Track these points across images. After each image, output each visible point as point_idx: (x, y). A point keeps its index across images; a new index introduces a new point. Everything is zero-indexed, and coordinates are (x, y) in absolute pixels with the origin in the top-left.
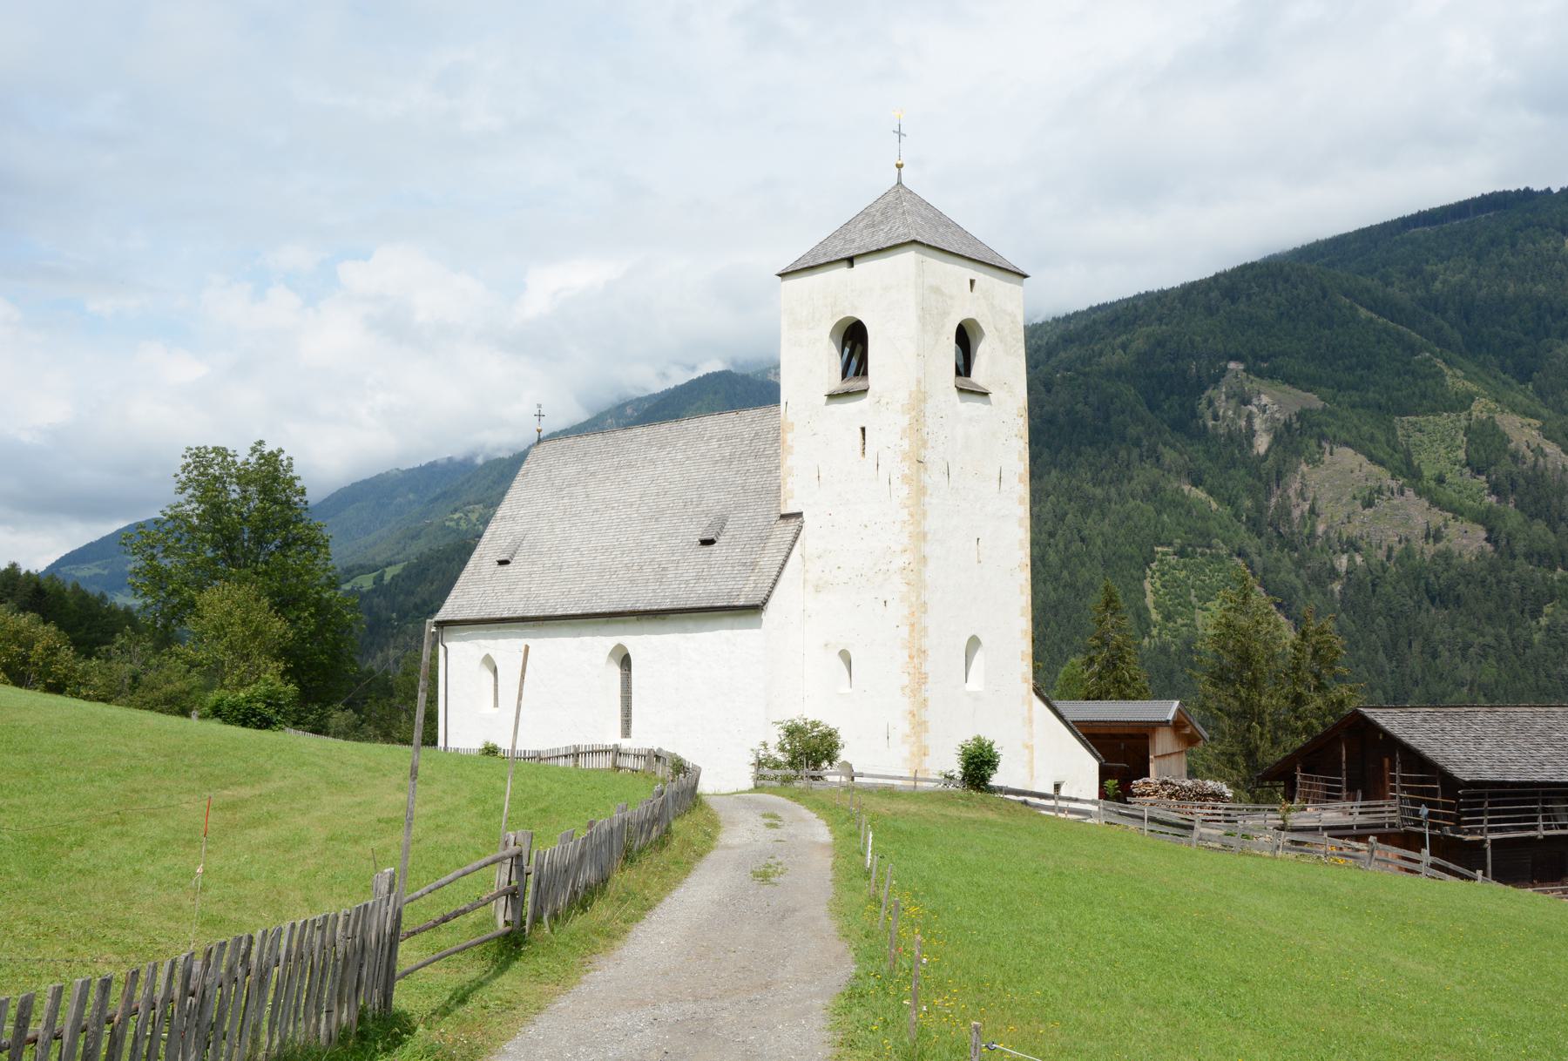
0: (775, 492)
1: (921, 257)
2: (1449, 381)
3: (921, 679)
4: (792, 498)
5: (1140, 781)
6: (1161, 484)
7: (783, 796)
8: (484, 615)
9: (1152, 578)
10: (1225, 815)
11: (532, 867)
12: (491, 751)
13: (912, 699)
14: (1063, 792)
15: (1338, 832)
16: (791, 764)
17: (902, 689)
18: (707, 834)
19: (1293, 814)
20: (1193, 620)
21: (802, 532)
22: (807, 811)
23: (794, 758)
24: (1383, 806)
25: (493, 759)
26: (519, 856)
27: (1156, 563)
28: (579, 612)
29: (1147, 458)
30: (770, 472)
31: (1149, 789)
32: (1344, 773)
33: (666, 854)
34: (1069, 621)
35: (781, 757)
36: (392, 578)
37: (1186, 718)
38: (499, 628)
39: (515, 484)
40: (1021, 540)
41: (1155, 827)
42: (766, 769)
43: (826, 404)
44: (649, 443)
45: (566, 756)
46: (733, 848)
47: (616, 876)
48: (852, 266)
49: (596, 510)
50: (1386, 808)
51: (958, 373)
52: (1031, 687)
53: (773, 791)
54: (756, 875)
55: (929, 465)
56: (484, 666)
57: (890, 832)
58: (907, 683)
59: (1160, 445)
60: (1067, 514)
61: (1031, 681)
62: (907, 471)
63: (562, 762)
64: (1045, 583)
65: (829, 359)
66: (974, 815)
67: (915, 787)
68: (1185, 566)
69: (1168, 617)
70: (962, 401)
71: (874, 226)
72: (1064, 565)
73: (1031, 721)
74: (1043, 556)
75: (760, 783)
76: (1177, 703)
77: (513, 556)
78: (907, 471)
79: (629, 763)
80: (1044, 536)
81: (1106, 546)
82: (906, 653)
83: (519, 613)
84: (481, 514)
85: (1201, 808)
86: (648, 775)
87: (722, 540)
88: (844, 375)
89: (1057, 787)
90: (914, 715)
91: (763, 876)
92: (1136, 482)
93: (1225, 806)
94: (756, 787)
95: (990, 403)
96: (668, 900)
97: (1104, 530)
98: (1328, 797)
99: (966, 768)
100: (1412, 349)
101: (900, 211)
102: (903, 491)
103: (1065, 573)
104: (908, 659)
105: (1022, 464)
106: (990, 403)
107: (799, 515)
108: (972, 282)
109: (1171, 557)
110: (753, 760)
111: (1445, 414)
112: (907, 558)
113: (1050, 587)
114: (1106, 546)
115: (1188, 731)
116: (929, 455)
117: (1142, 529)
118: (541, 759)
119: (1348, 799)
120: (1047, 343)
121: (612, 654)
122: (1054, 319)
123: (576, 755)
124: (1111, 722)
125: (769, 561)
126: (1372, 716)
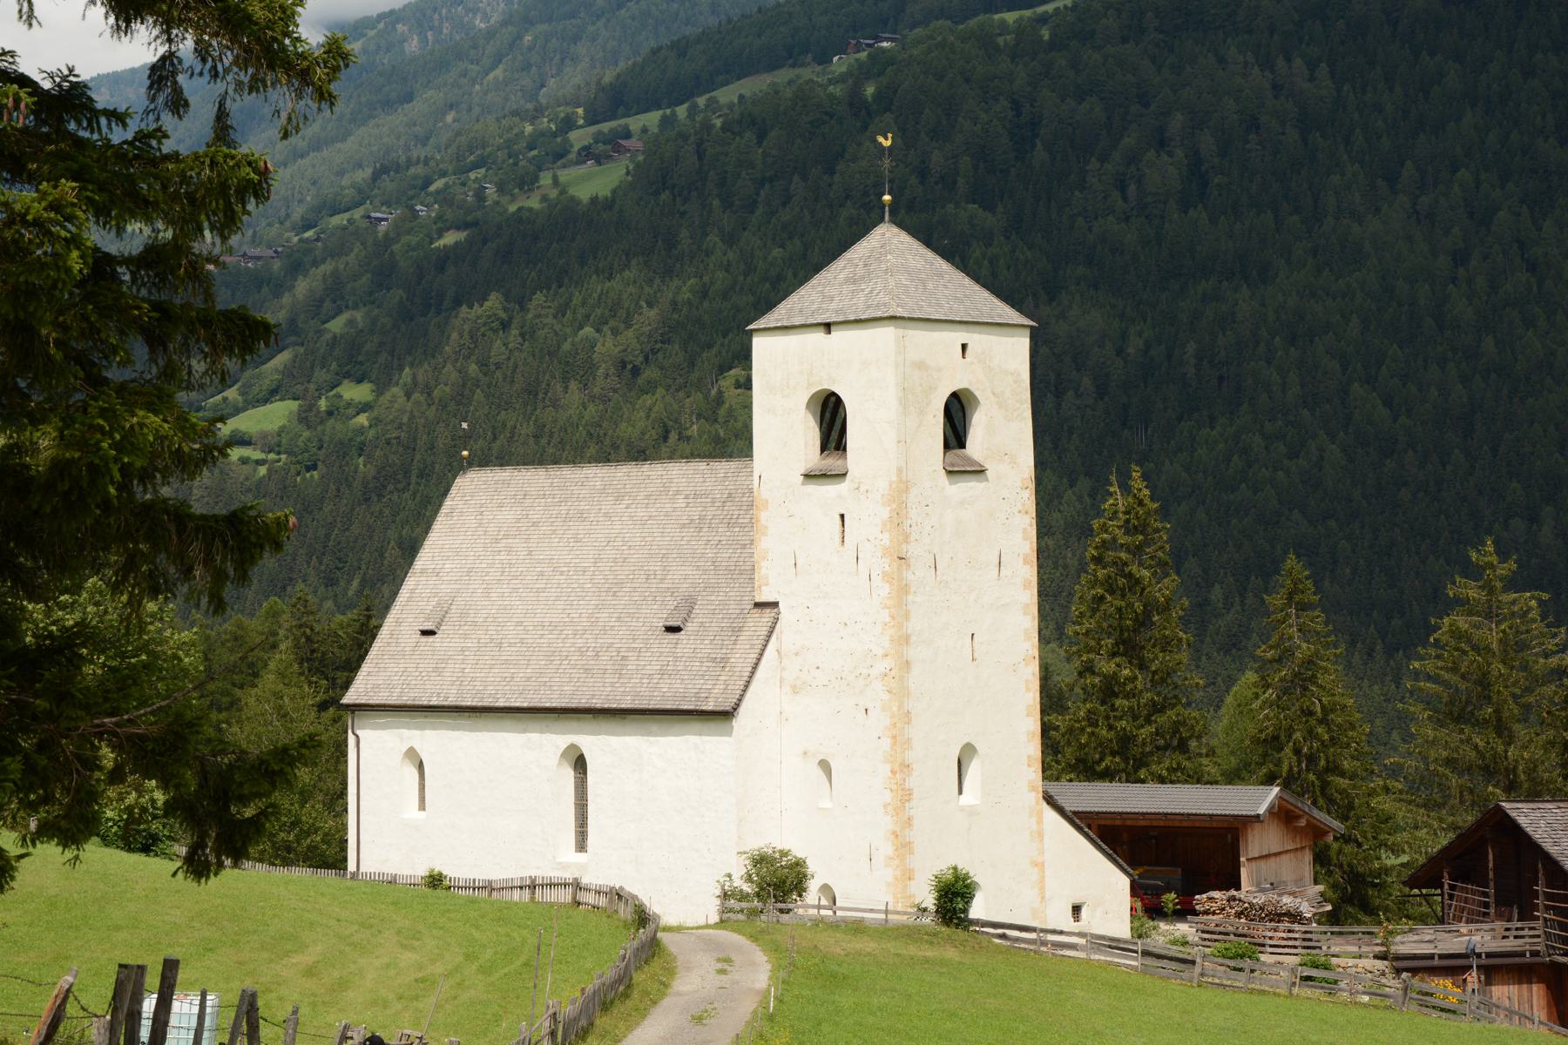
0: (747, 573)
1: (901, 332)
4: (767, 585)
5: (1204, 896)
7: (744, 935)
8: (406, 699)
10: (1304, 940)
12: (435, 881)
15: (1453, 967)
16: (758, 895)
17: (885, 806)
19: (1398, 938)
21: (778, 626)
22: (761, 953)
23: (762, 889)
24: (1522, 929)
25: (439, 892)
26: (555, 1014)
28: (525, 705)
32: (1492, 884)
33: (629, 1003)
35: (747, 888)
42: (732, 901)
43: (803, 484)
45: (521, 888)
47: (597, 1022)
48: (830, 333)
49: (541, 574)
50: (1526, 932)
54: (693, 1017)
57: (830, 977)
62: (887, 568)
63: (516, 895)
65: (809, 431)
66: (930, 953)
67: (886, 920)
71: (854, 282)
73: (1040, 835)
75: (725, 916)
76: (1276, 790)
79: (590, 898)
82: (888, 767)
83: (451, 701)
85: (1275, 931)
86: (611, 914)
87: (690, 627)
88: (823, 448)
89: (1076, 910)
90: (897, 836)
91: (698, 1020)
94: (722, 921)
95: (987, 480)
96: (630, 1036)
99: (939, 899)
102: (884, 590)
103: (1489, 343)
104: (890, 774)
105: (1028, 543)
106: (987, 480)
107: (775, 605)
108: (964, 347)
110: (718, 892)
115: (1303, 823)
116: (912, 550)
119: (1499, 916)
124: (1189, 815)
125: (741, 659)
126: (1513, 814)
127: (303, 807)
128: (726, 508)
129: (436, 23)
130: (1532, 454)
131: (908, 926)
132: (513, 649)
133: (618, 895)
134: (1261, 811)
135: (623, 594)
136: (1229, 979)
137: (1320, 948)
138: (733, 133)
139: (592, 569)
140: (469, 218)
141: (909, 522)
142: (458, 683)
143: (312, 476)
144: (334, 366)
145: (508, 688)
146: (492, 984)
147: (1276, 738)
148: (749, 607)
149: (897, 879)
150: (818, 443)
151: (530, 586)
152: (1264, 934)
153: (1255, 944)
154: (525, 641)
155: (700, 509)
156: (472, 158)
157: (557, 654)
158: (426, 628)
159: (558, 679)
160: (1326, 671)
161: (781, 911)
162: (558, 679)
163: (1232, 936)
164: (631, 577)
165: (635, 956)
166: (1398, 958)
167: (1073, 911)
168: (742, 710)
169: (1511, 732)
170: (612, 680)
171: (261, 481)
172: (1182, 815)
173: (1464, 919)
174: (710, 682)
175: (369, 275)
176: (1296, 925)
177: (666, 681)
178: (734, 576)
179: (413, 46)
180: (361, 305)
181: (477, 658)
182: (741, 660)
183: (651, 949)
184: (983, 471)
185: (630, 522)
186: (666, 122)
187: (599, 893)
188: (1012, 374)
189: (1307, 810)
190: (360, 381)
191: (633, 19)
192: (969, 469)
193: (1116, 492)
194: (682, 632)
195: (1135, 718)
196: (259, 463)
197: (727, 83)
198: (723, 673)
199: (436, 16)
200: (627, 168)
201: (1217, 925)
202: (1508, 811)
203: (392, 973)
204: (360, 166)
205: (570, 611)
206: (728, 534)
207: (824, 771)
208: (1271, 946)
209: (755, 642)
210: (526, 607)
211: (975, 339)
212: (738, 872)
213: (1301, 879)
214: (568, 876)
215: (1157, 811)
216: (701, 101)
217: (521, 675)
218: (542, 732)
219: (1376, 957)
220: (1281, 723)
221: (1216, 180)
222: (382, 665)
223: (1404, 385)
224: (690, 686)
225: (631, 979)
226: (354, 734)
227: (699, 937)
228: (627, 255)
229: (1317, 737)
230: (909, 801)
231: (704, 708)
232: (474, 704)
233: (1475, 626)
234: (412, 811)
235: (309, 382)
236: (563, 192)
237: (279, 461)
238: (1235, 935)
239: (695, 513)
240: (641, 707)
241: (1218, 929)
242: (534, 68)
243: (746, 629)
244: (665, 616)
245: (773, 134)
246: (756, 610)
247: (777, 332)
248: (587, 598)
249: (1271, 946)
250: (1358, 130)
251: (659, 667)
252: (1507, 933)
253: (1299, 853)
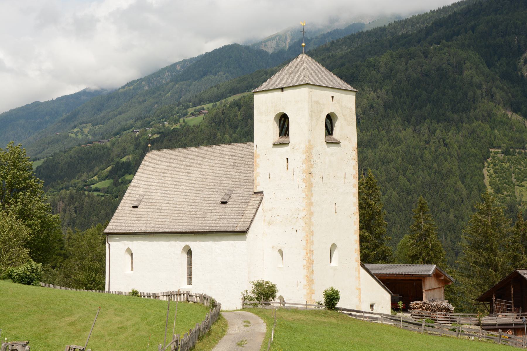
0: (252, 182)
1: (310, 90)
3: (311, 263)
4: (259, 185)
5: (414, 302)
6: (494, 111)
9: (488, 167)
10: (451, 318)
11: (180, 343)
12: (135, 293)
13: (307, 271)
15: (505, 327)
16: (257, 298)
17: (304, 266)
18: (223, 330)
19: (484, 318)
20: (514, 192)
21: (263, 200)
22: (261, 319)
23: (259, 296)
25: (136, 297)
26: (177, 340)
27: (491, 158)
28: (170, 231)
29: (486, 96)
30: (250, 173)
31: (418, 306)
32: (513, 299)
34: (437, 193)
35: (253, 296)
36: (37, 168)
37: (441, 272)
38: (134, 237)
39: (139, 170)
40: (354, 203)
41: (405, 324)
43: (273, 148)
44: (198, 156)
45: (167, 296)
46: (232, 335)
49: (176, 185)
52: (359, 263)
53: (250, 310)
55: (314, 175)
56: (127, 253)
59: (494, 88)
60: (436, 130)
61: (359, 261)
62: (305, 177)
64: (423, 171)
65: (275, 129)
67: (306, 308)
68: (509, 160)
69: (498, 191)
70: (328, 147)
71: (292, 74)
72: (435, 160)
73: (359, 278)
74: (422, 155)
75: (244, 306)
76: (435, 266)
77: (139, 204)
78: (305, 177)
79: (193, 299)
80: (423, 143)
81: (460, 149)
82: (305, 251)
84: (90, 129)
85: (440, 315)
86: (201, 304)
87: (230, 202)
88: (280, 135)
89: (372, 306)
90: (308, 277)
91: (240, 344)
92: (478, 110)
93: (451, 314)
94: (243, 308)
95: (340, 147)
97: (459, 139)
98: (508, 310)
99: (326, 300)
101: (303, 67)
102: (303, 185)
103: (435, 165)
106: (340, 147)
108: (332, 97)
109: (500, 155)
110: (242, 297)
112: (305, 213)
113: (426, 172)
114: (460, 149)
115: (442, 278)
116: (314, 171)
117: (482, 138)
118: (156, 297)
119: (515, 311)
120: (426, 27)
121: (184, 249)
122: (431, 11)
123: (171, 295)
124: (404, 274)
125: (249, 212)
126: (522, 274)
127: (96, 275)
128: (243, 160)
129: (153, 82)
130: (447, 195)
131: (315, 310)
132: (165, 212)
133: (204, 297)
134: (431, 273)
135: (206, 191)
136: (435, 331)
137: (456, 321)
138: (232, 108)
139: (194, 183)
140: (161, 131)
141: (313, 160)
142: (146, 224)
143: (117, 199)
144: (123, 170)
145: (163, 225)
146: (152, 330)
147: (416, 255)
148: (252, 194)
149: (308, 294)
150: (278, 133)
151: (172, 190)
152: (436, 316)
153: (433, 320)
154: (170, 209)
155: (234, 160)
156: (162, 116)
157: (181, 213)
158: (134, 205)
159: (182, 222)
160: (432, 233)
161: (266, 304)
162: (182, 222)
163: (424, 317)
164: (209, 185)
165: (212, 318)
166: (484, 325)
167: (371, 306)
168: (250, 231)
169: (496, 252)
170: (201, 221)
171: (103, 201)
172: (402, 274)
173: (500, 312)
174: (237, 221)
175: (133, 146)
176: (448, 313)
177: (221, 221)
178: (247, 183)
179: (146, 88)
180: (131, 154)
181: (152, 215)
182: (250, 213)
183: (218, 316)
184: (339, 143)
185: (208, 166)
186: (213, 106)
187: (196, 297)
188: (349, 108)
189: (444, 273)
190: (130, 174)
191: (205, 80)
192: (334, 142)
193: (363, 177)
194: (227, 204)
195: (369, 249)
196: (102, 196)
197: (230, 96)
198: (243, 218)
199: (153, 80)
200: (203, 117)
201: (419, 313)
202: (520, 273)
203: (109, 324)
204: (132, 119)
205: (186, 198)
206: (244, 168)
207: (280, 253)
208: (439, 320)
209: (255, 206)
210: (170, 197)
211: (337, 94)
212: (250, 288)
213: (441, 298)
214: (185, 291)
215: (393, 273)
216: (223, 101)
217: (168, 221)
218: (175, 241)
219: (476, 325)
220: (418, 250)
221: (362, 121)
222: (119, 219)
223: (413, 176)
224: (230, 223)
225: (210, 328)
226: (108, 243)
227: (235, 313)
228: (203, 140)
229: (430, 255)
230: (312, 264)
231: (235, 230)
232: (151, 231)
233: (483, 218)
234: (128, 271)
235: (116, 174)
236: (186, 124)
237: (108, 195)
238: (426, 316)
239: (232, 162)
240: (212, 230)
241: (419, 314)
242: (179, 93)
243: (251, 201)
244: (221, 198)
245: (243, 108)
247: (263, 92)
248: (193, 193)
249: (439, 320)
250: (400, 108)
251: (219, 216)
252: (517, 317)
253: (440, 289)
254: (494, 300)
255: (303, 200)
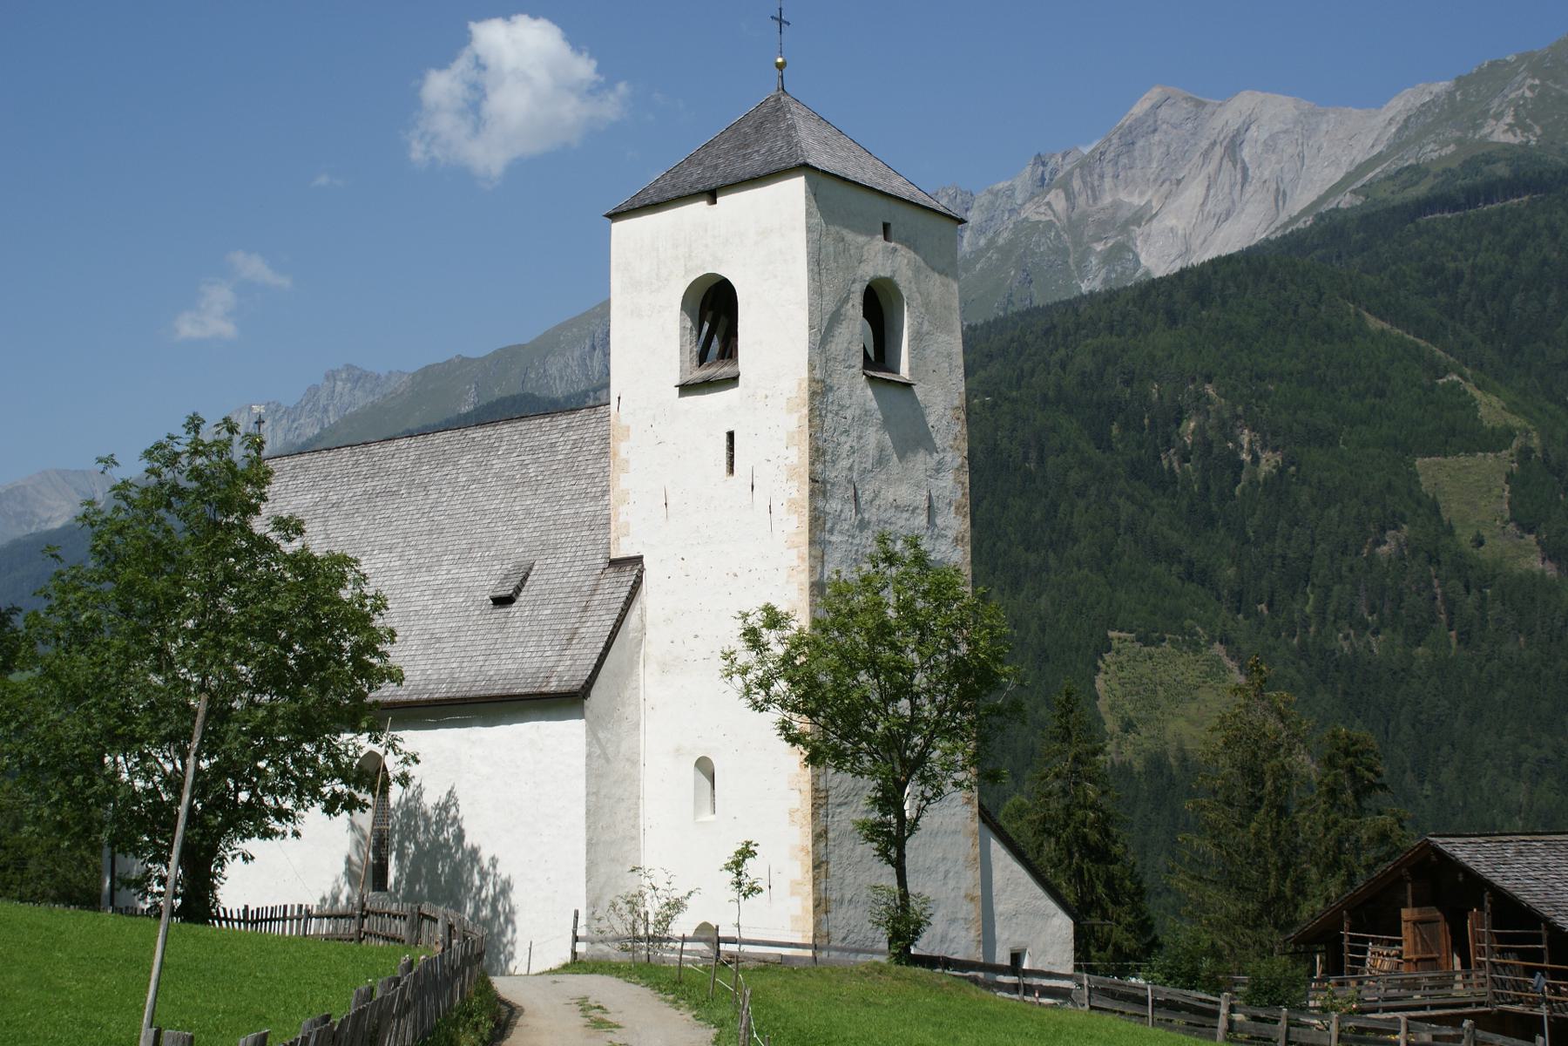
2: (1482, 411)
4: (627, 535)
14: (1026, 965)
17: (792, 813)
48: (715, 203)
51: (868, 363)
58: (797, 805)
88: (702, 358)
100: (1438, 370)
111: (1480, 454)
126: (1448, 849)
139: (401, 545)
148: (602, 566)
168: (594, 692)
246: (611, 570)
254: (1346, 939)
255: (789, 576)
